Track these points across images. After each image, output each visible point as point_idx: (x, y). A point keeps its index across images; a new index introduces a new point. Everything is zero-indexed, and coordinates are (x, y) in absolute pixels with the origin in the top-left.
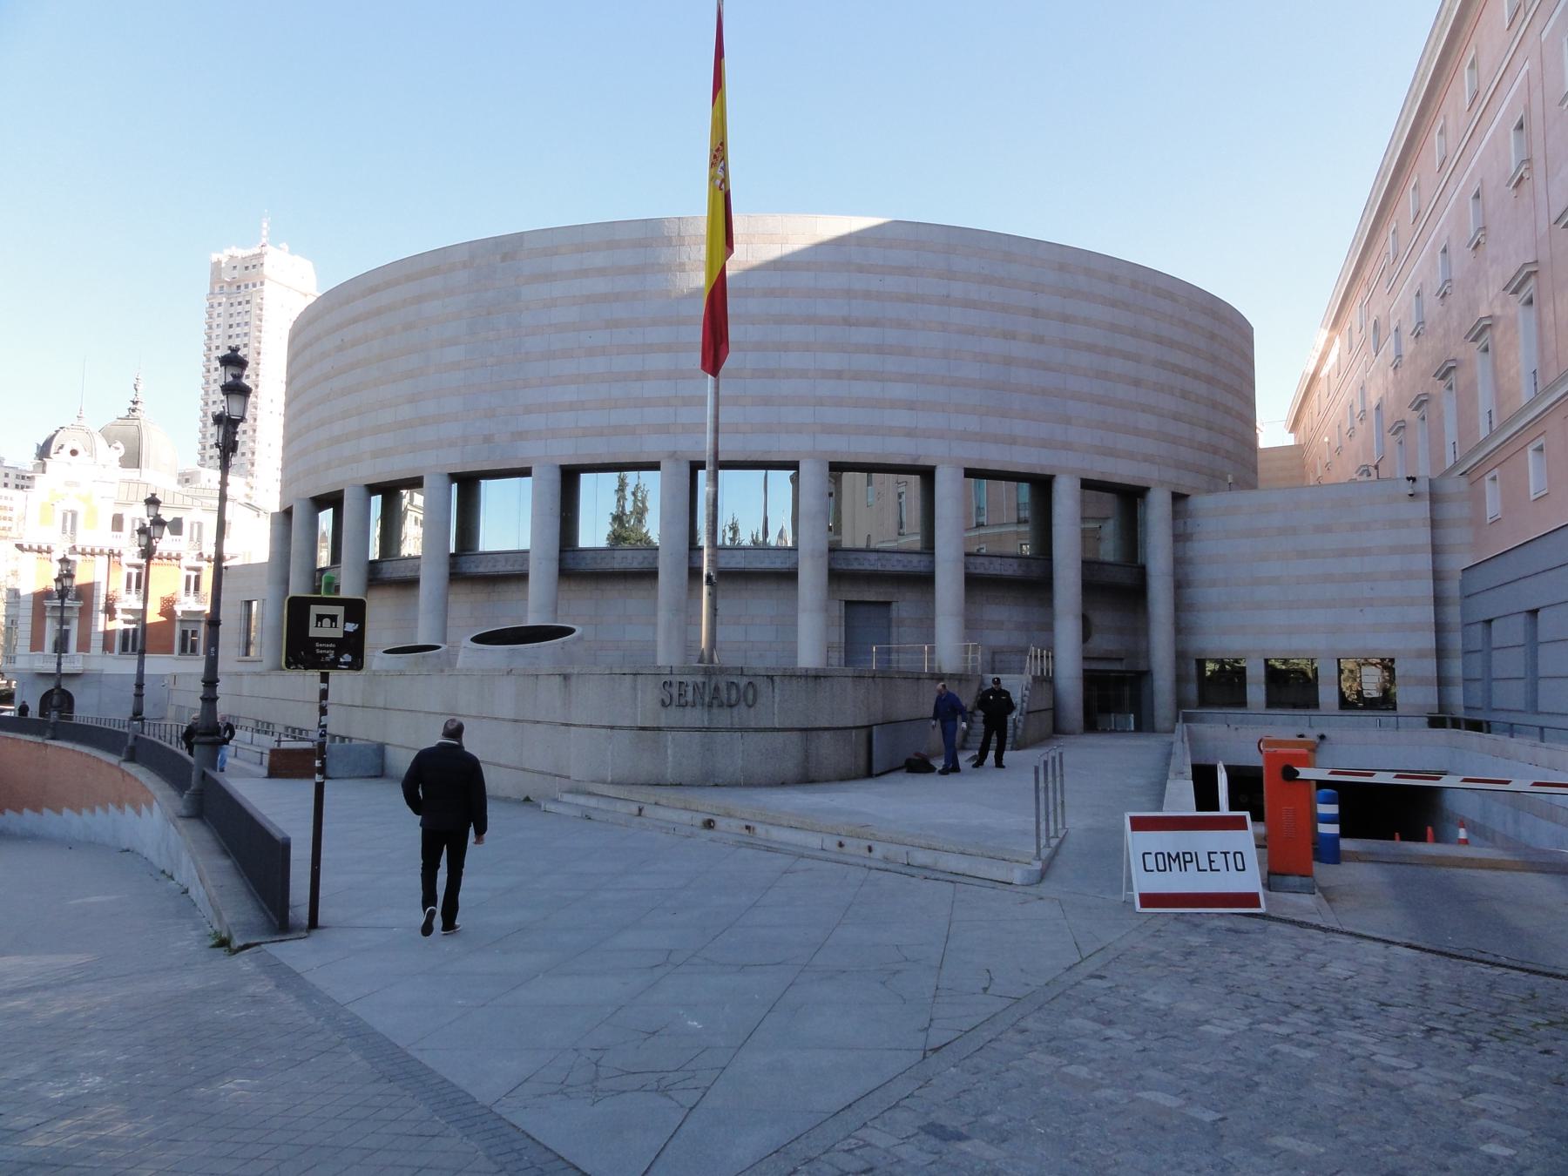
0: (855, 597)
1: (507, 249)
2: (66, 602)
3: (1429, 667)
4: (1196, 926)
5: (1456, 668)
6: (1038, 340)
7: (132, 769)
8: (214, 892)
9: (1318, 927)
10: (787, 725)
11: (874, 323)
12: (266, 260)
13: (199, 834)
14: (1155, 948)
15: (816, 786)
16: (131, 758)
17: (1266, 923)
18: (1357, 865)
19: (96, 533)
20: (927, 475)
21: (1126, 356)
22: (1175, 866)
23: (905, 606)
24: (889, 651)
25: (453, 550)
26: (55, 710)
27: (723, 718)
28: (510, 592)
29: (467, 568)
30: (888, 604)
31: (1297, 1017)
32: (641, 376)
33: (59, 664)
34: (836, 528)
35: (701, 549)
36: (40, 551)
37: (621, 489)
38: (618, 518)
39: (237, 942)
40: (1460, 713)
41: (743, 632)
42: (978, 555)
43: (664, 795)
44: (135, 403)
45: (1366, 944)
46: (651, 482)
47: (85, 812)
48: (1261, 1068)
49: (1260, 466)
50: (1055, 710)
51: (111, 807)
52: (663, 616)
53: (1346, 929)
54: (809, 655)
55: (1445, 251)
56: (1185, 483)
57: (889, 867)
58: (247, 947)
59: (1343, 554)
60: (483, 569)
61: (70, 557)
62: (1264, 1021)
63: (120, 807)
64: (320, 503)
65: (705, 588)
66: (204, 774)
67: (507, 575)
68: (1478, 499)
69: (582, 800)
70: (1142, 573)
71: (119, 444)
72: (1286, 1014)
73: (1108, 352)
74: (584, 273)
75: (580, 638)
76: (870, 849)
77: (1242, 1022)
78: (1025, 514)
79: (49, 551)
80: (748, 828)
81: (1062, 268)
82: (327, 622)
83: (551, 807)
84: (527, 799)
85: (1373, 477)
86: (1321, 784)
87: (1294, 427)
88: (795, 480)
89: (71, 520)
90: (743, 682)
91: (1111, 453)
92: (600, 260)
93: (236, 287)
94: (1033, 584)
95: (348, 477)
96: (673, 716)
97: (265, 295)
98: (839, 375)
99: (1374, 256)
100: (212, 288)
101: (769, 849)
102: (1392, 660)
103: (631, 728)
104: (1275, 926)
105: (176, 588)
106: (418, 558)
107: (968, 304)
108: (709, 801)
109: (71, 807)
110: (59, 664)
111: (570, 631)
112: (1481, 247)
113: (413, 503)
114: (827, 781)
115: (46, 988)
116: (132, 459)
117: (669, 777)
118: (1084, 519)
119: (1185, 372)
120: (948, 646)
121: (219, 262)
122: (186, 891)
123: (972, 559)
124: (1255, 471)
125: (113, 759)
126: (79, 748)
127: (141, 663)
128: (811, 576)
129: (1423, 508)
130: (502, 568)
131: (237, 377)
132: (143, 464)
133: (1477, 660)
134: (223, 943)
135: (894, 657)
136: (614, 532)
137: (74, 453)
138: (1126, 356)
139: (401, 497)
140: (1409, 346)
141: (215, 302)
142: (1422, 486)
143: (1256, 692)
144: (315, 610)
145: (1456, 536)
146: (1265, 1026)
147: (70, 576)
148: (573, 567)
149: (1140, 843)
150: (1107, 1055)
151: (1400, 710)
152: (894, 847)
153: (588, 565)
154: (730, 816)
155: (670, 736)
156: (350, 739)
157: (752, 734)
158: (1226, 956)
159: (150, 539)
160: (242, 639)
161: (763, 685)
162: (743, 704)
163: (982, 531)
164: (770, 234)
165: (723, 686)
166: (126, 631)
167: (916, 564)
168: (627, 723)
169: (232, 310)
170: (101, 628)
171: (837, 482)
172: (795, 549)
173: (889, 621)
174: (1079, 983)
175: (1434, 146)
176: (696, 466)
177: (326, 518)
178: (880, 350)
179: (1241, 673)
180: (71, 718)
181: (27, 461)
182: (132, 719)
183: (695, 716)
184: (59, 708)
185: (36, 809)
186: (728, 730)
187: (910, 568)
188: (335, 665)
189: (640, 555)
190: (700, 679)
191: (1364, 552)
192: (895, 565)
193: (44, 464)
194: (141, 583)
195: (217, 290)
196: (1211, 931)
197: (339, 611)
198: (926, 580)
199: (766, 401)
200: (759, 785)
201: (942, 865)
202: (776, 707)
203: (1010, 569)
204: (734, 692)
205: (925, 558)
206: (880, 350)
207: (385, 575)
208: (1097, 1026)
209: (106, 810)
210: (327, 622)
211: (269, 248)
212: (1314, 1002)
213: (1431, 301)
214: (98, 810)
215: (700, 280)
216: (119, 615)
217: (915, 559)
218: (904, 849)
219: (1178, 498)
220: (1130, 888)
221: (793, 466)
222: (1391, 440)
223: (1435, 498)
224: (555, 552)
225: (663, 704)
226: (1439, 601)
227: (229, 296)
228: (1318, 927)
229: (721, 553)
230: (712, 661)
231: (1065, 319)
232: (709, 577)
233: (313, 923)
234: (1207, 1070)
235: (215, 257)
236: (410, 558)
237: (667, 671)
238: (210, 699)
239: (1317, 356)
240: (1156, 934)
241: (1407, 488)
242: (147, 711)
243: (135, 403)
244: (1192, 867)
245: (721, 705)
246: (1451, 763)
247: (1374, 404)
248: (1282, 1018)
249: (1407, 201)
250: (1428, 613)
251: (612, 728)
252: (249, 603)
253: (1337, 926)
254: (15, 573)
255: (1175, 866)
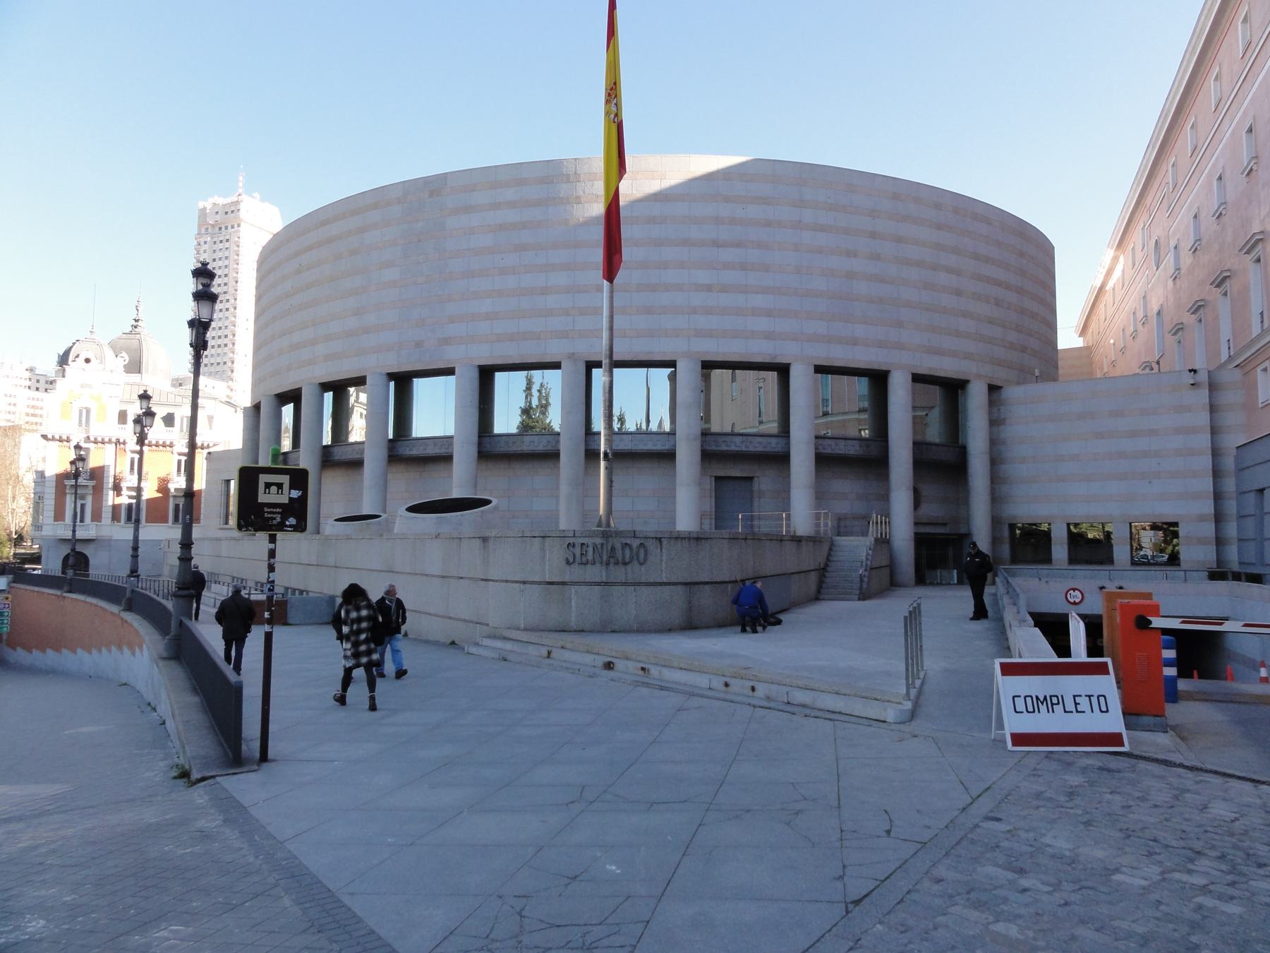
0: (722, 474)
1: (434, 187)
2: (80, 482)
3: (1209, 529)
4: (1069, 764)
5: (1231, 530)
6: (876, 257)
7: (130, 617)
8: (181, 728)
9: (1181, 766)
10: (673, 580)
11: (739, 245)
12: (242, 206)
13: (177, 672)
14: (1039, 788)
15: (697, 633)
16: (129, 608)
17: (1134, 761)
18: (1192, 703)
19: (105, 426)
20: (783, 371)
21: (950, 270)
22: (1043, 708)
23: (765, 480)
24: (752, 518)
25: (391, 436)
26: (76, 567)
27: (619, 573)
28: (436, 471)
29: (402, 451)
30: (751, 479)
31: (1203, 864)
32: (545, 291)
33: (74, 531)
34: (707, 418)
35: (599, 433)
36: (61, 440)
37: (529, 388)
38: (526, 411)
39: (195, 775)
40: (1235, 567)
41: (630, 502)
42: (824, 437)
43: (567, 639)
44: (137, 321)
45: (1234, 783)
46: (553, 380)
47: (94, 651)
48: (1195, 926)
49: (1060, 363)
50: (892, 567)
51: (113, 648)
52: (564, 489)
53: (1209, 767)
54: (686, 518)
55: (1220, 178)
56: (999, 376)
57: (771, 705)
58: (203, 779)
59: (1134, 434)
60: (415, 452)
61: (83, 445)
62: (1174, 871)
63: (120, 648)
64: (283, 398)
65: (602, 464)
66: (181, 624)
67: (436, 457)
68: (1251, 389)
69: (499, 644)
70: (963, 452)
71: (124, 354)
72: (1192, 861)
73: (935, 267)
74: (495, 206)
75: (496, 508)
76: (753, 689)
77: (1153, 871)
78: (866, 404)
79: (68, 440)
80: (643, 669)
81: (896, 197)
82: (274, 489)
83: (473, 650)
84: (453, 643)
85: (1156, 370)
86: (1165, 631)
87: (1083, 332)
88: (673, 378)
89: (85, 415)
90: (635, 543)
91: (939, 352)
92: (510, 194)
93: (219, 225)
94: (873, 461)
95: (306, 377)
96: (576, 573)
97: (241, 235)
98: (709, 288)
99: (1156, 186)
100: (199, 229)
101: (662, 688)
102: (1176, 524)
103: (540, 583)
104: (1142, 765)
105: (162, 469)
106: (363, 443)
107: (822, 229)
108: (611, 645)
109: (83, 648)
110: (74, 531)
111: (488, 502)
112: (1253, 173)
113: (358, 399)
114: (708, 627)
115: (20, 819)
116: (135, 366)
117: (573, 625)
118: (914, 408)
119: (999, 284)
120: (802, 513)
121: (205, 209)
122: (164, 723)
123: (820, 441)
124: (1057, 367)
125: (114, 609)
126: (89, 599)
127: (137, 530)
128: (687, 456)
129: (1204, 394)
130: (431, 451)
131: (207, 286)
132: (144, 370)
133: (1250, 524)
134: (184, 775)
135: (756, 523)
136: (522, 423)
137: (88, 361)
138: (950, 270)
139: (347, 396)
140: (1187, 260)
141: (202, 241)
142: (1203, 377)
143: (1060, 551)
144: (264, 479)
145: (1231, 419)
146: (1177, 875)
147: (81, 459)
148: (491, 450)
149: (1009, 686)
150: (1032, 910)
151: (1184, 565)
152: (774, 687)
153: (502, 448)
154: (627, 659)
155: (573, 589)
156: (308, 592)
157: (644, 589)
158: (1109, 796)
159: (143, 427)
160: (223, 511)
161: (652, 546)
162: (636, 562)
163: (829, 419)
164: (655, 171)
165: (618, 546)
166: (130, 505)
167: (774, 445)
168: (537, 579)
169: (215, 247)
170: (110, 503)
171: (706, 379)
172: (672, 433)
173: (752, 491)
174: (976, 826)
175: (1210, 90)
176: (591, 365)
177: (288, 410)
178: (744, 267)
179: (1047, 535)
180: (88, 576)
181: (48, 366)
182: (129, 576)
183: (595, 573)
184: (74, 567)
185: (57, 649)
186: (625, 584)
187: (768, 449)
188: (281, 527)
189: (544, 440)
190: (598, 541)
191: (1152, 433)
192: (757, 446)
193: (64, 370)
194: (139, 467)
195: (203, 231)
196: (1084, 770)
197: (285, 479)
198: (781, 459)
199: (649, 311)
200: (650, 631)
201: (819, 704)
202: (664, 564)
203: (852, 449)
204: (627, 552)
205: (782, 441)
206: (744, 267)
207: (339, 459)
208: (1010, 875)
209: (110, 651)
210: (274, 489)
211: (244, 196)
212: (1213, 847)
213: (1208, 222)
214: (104, 651)
215: (598, 209)
216: (125, 492)
217: (774, 441)
218: (784, 689)
219: (993, 389)
220: (1001, 726)
221: (671, 364)
222: (1170, 340)
223: (1213, 387)
224: (475, 439)
225: (568, 562)
226: (1217, 473)
227: (213, 235)
228: (1181, 766)
229: (615, 437)
230: (608, 525)
231: (899, 240)
232: (606, 454)
233: (264, 757)
234: (1140, 929)
235: (201, 205)
236: (356, 443)
237: (571, 534)
238: (186, 559)
239: (1104, 271)
240: (1035, 774)
241: (1190, 379)
242: (143, 569)
243: (137, 321)
244: (1058, 709)
245: (617, 563)
246: (1239, 613)
247: (1155, 310)
248: (1191, 866)
249: (1186, 139)
250: (1207, 484)
251: (524, 583)
252: (228, 482)
253: (1199, 765)
254: (44, 460)
255: (1043, 708)
